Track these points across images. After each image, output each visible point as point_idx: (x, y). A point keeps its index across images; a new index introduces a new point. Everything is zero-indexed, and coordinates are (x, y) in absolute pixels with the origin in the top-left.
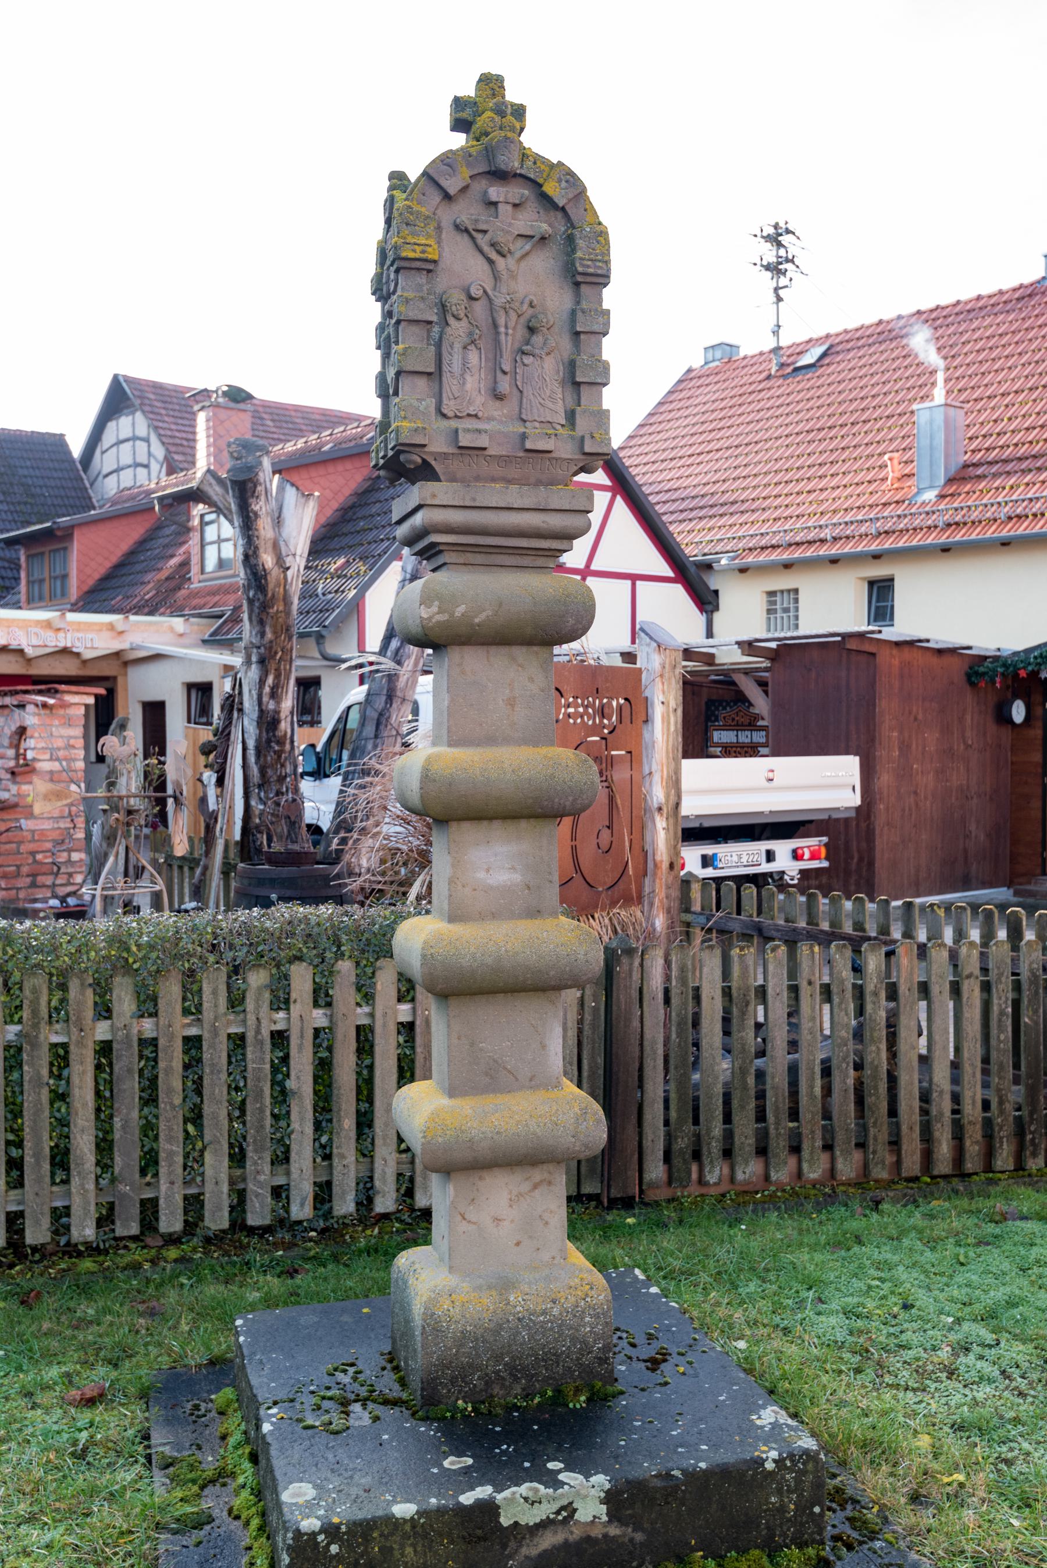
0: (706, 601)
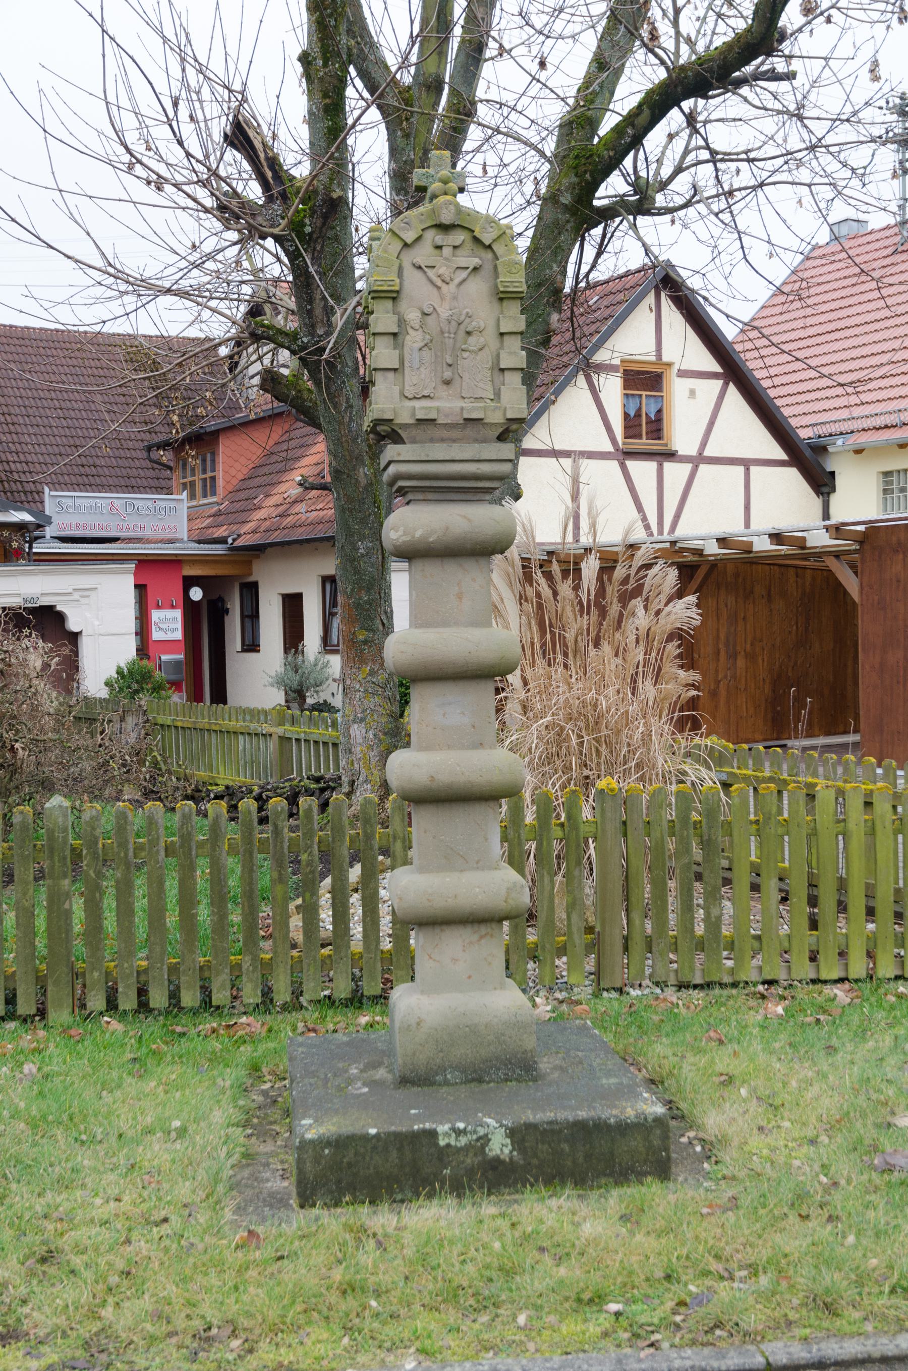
0: (822, 483)
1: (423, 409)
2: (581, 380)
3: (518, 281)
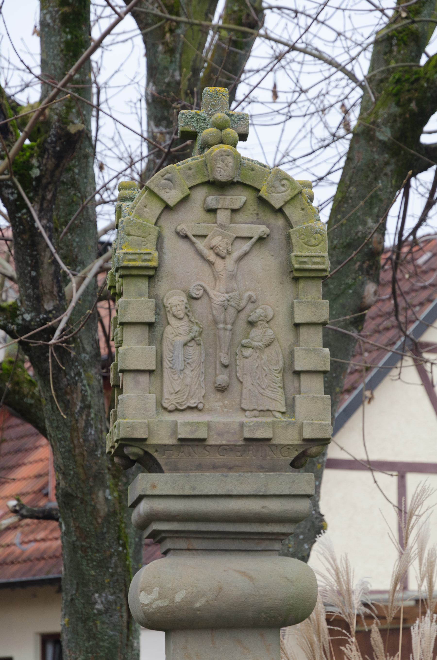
1: (187, 424)
2: (408, 361)
3: (318, 255)
